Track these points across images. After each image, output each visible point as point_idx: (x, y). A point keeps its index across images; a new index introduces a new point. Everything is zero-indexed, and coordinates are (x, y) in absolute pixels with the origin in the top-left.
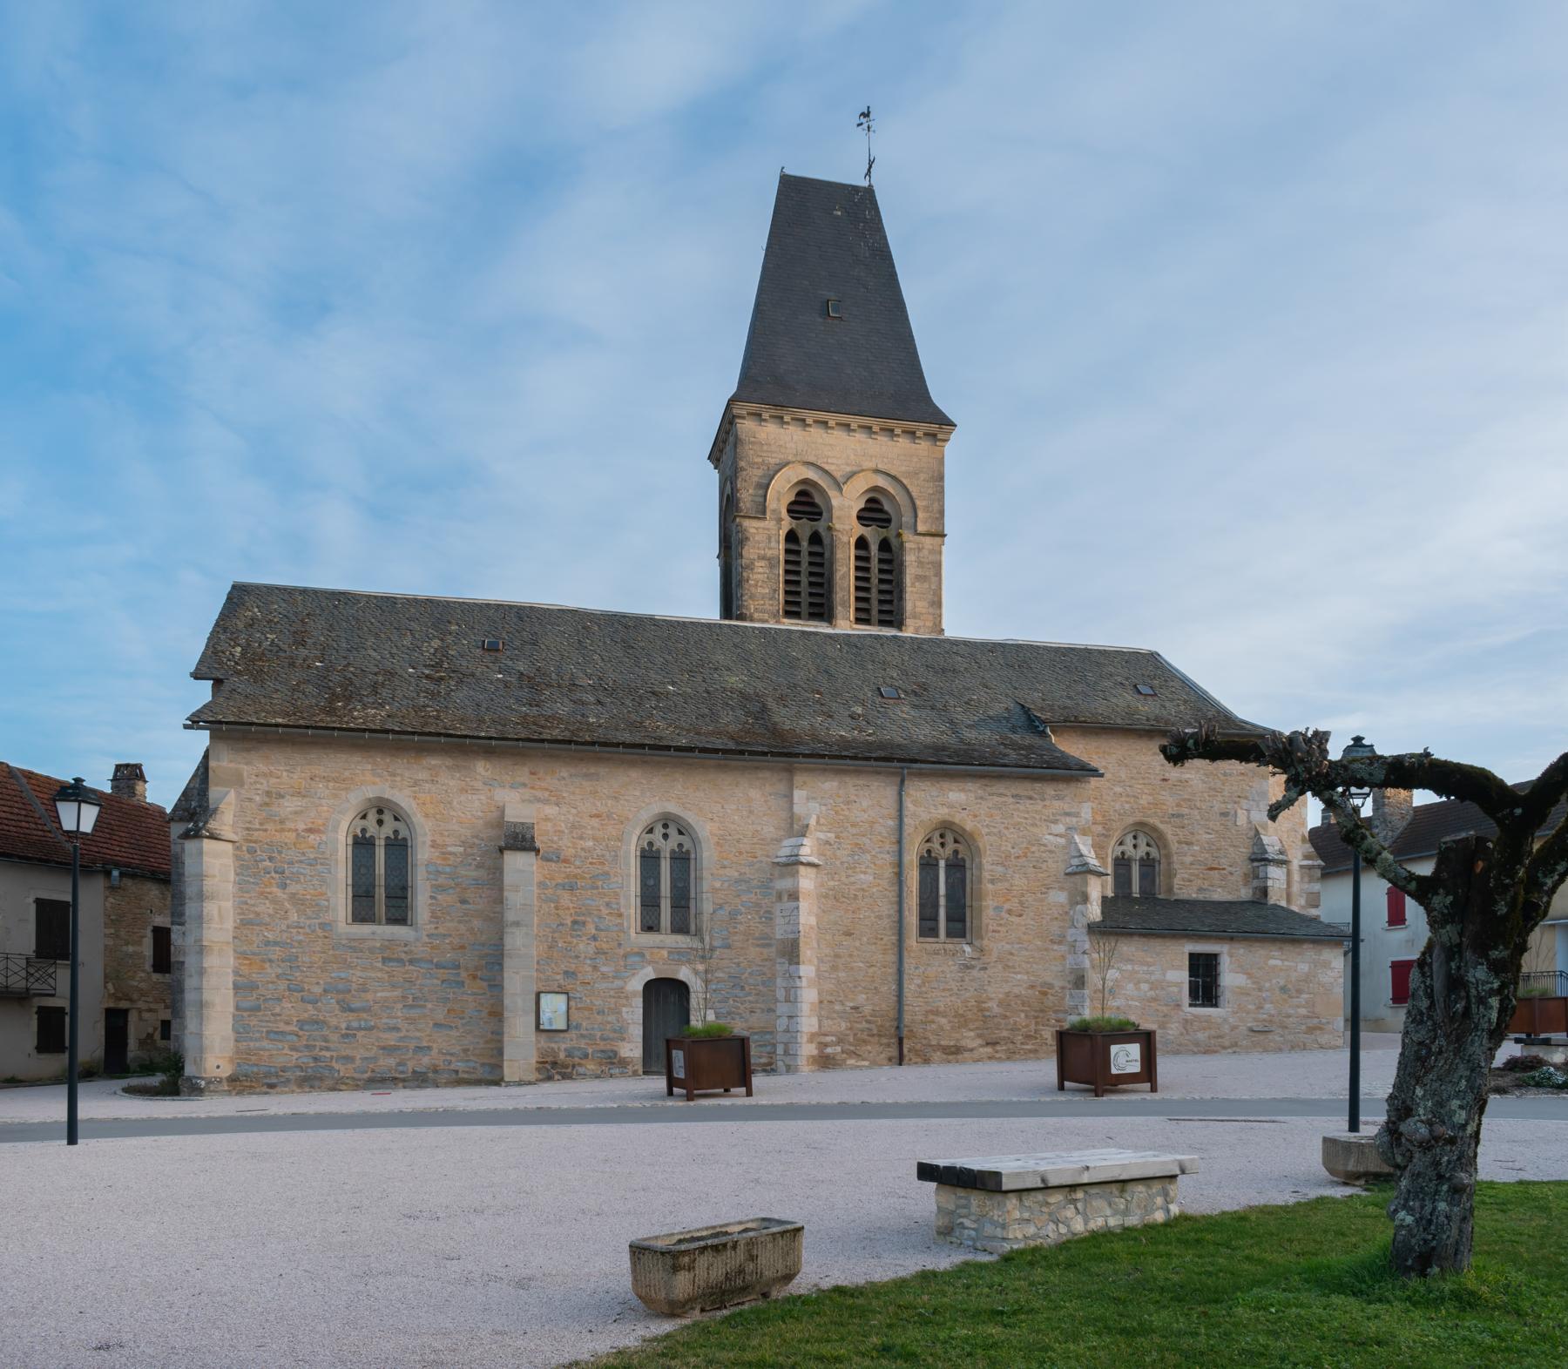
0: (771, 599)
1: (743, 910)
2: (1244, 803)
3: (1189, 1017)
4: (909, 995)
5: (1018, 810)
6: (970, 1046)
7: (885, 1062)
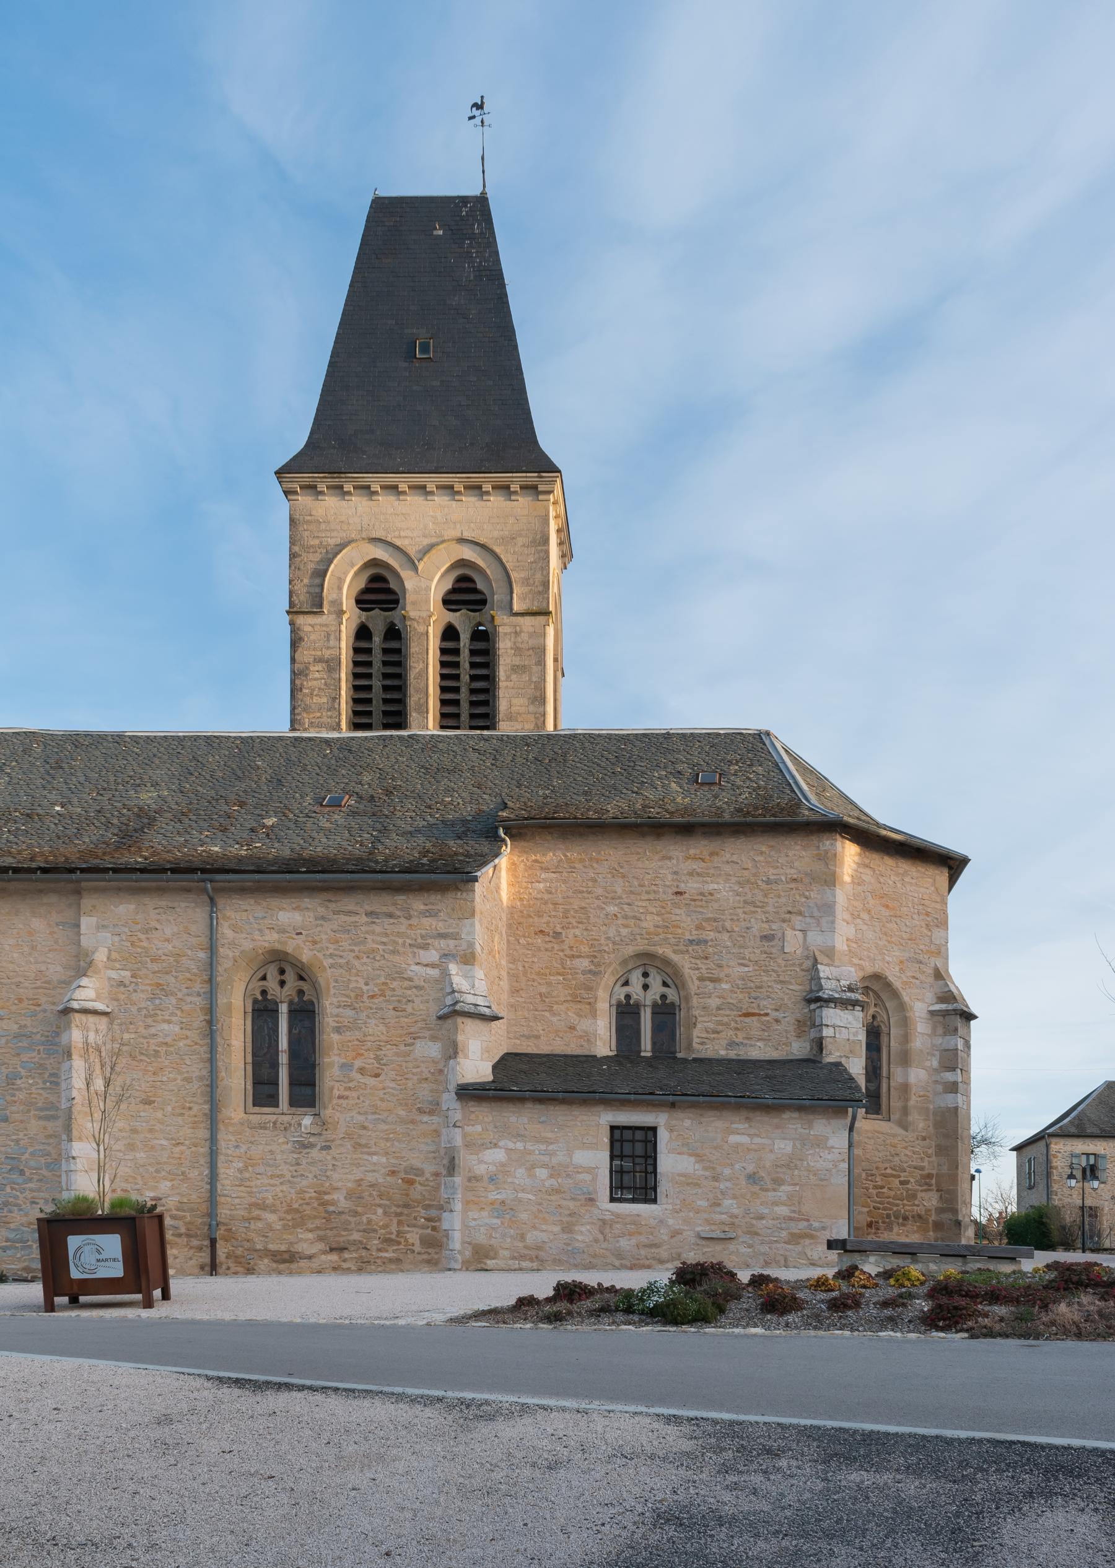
0: (329, 710)
1: (23, 1072)
2: (797, 920)
3: (608, 1217)
4: (227, 1182)
5: (373, 932)
6: (308, 1253)
7: (196, 1270)
